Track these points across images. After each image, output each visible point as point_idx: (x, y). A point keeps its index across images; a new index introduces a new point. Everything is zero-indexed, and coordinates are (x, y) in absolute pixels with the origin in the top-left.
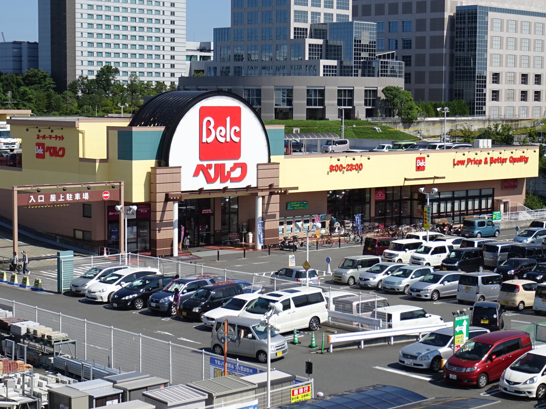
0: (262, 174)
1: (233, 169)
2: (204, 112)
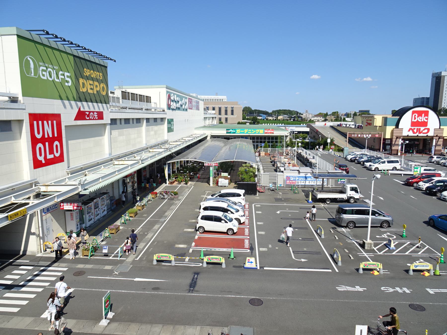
0: (436, 132)
1: (424, 130)
2: (413, 112)
